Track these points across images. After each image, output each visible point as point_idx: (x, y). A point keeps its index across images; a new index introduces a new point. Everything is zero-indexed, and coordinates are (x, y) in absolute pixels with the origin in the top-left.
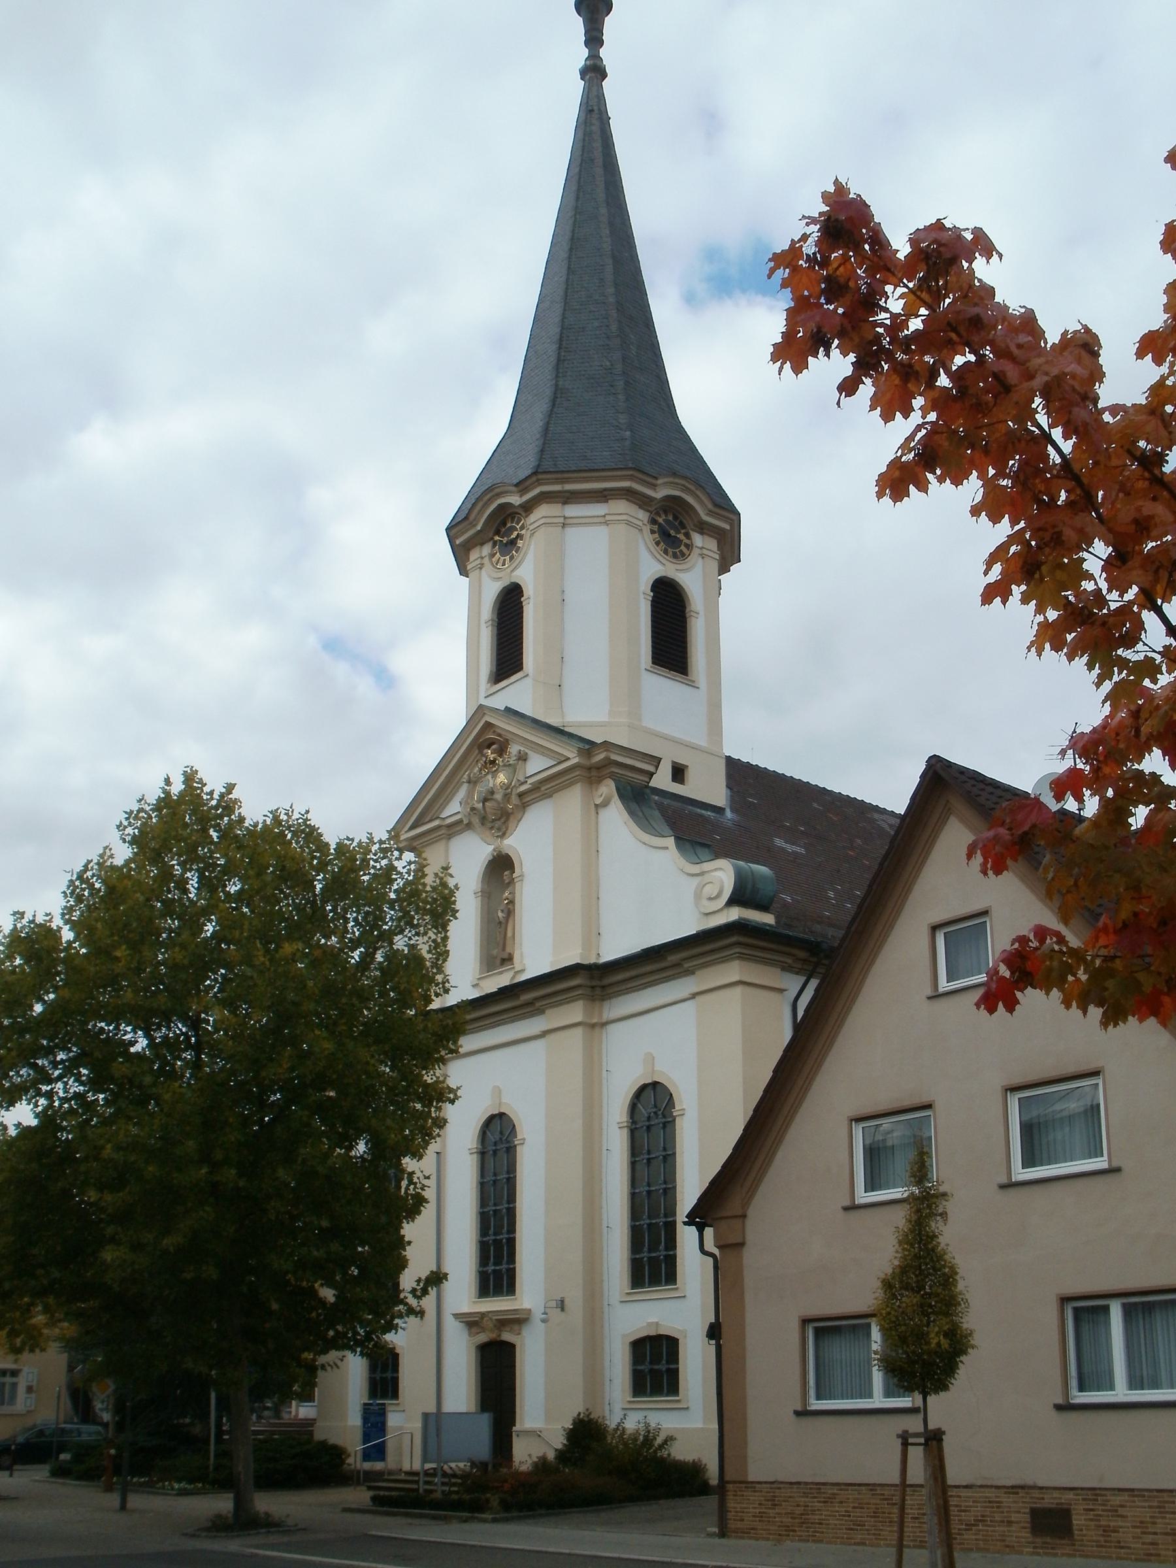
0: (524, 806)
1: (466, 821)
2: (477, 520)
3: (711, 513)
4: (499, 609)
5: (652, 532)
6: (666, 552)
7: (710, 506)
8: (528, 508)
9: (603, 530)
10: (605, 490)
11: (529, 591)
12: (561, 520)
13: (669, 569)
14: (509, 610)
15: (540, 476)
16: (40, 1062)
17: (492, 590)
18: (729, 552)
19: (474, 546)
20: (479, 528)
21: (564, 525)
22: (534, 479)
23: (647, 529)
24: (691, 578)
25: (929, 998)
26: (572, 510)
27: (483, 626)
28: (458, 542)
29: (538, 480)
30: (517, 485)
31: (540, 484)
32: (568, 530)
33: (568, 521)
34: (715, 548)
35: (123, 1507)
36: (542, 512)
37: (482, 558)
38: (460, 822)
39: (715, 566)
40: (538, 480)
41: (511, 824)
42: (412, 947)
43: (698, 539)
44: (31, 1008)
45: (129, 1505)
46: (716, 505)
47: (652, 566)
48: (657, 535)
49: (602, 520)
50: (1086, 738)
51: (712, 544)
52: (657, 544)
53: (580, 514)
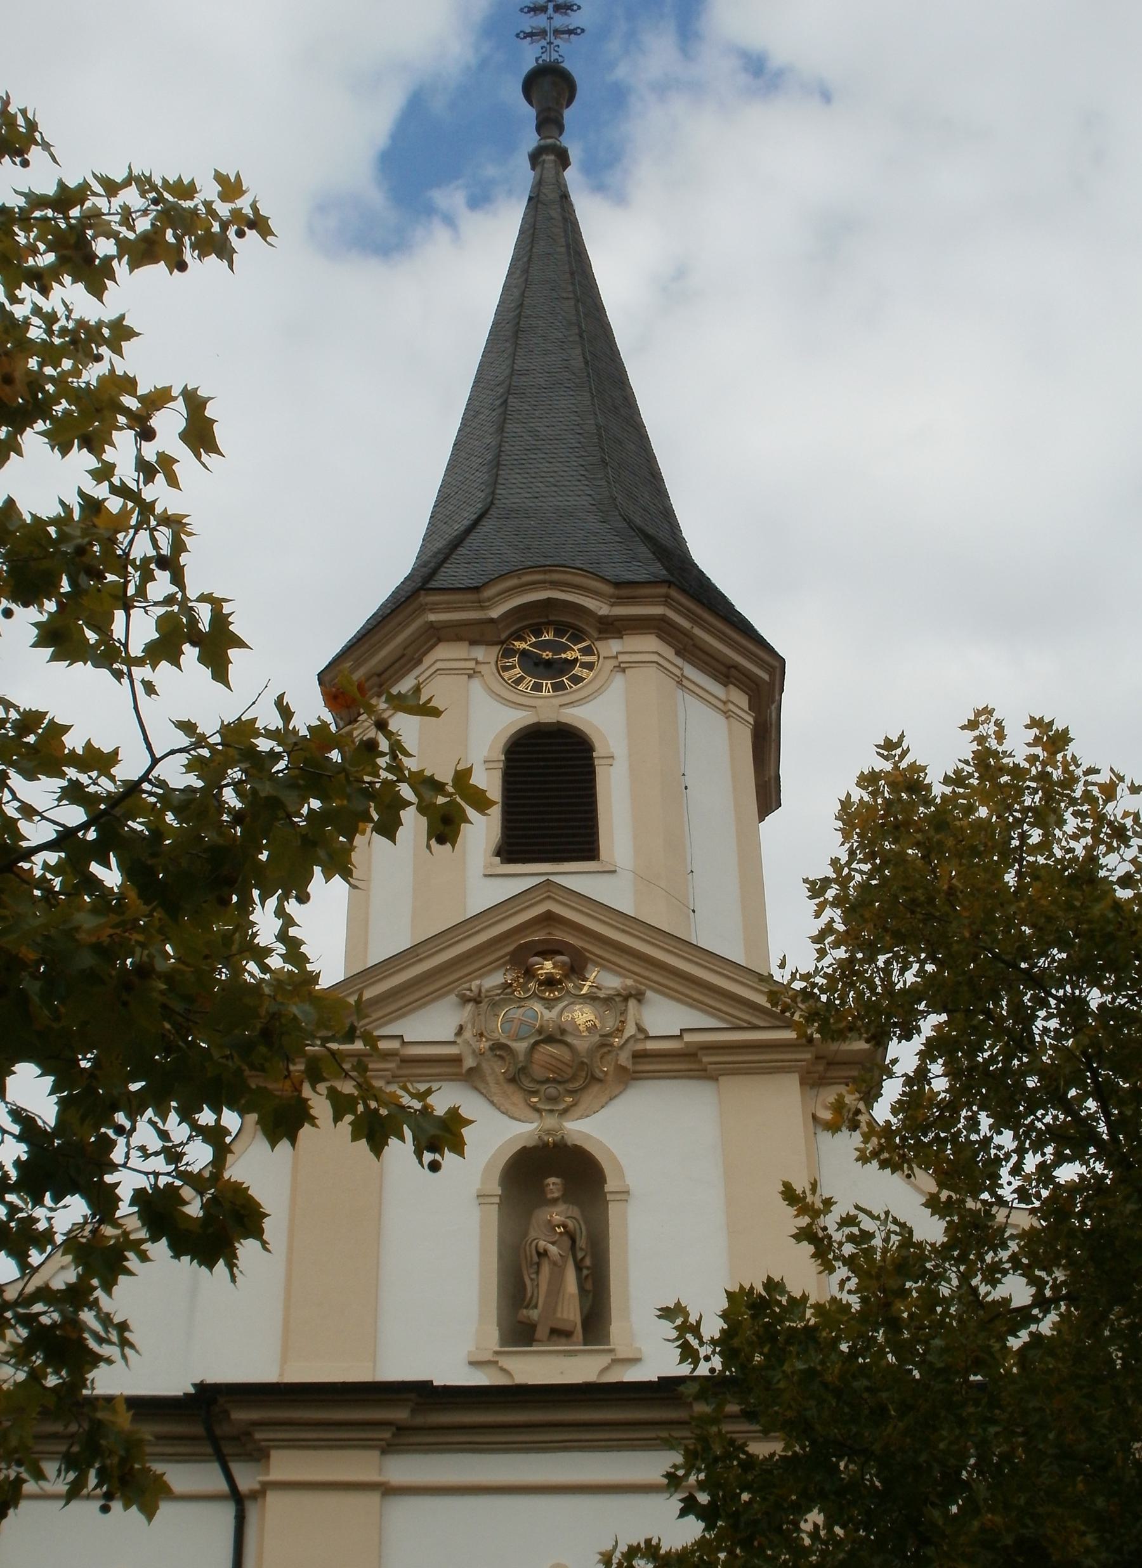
0: (628, 1077)
1: (469, 1062)
2: (493, 601)
3: (620, 600)
8: (612, 628)
10: (736, 667)
12: (472, 664)
13: (547, 706)
15: (673, 593)
19: (458, 639)
20: (494, 614)
21: (470, 676)
22: (663, 590)
25: (471, 1363)
29: (667, 596)
30: (617, 585)
31: (666, 604)
33: (685, 682)
38: (457, 1060)
40: (667, 596)
41: (587, 1099)
42: (1018, 1337)
44: (889, 1365)
46: (617, 585)
49: (720, 705)
53: (708, 688)
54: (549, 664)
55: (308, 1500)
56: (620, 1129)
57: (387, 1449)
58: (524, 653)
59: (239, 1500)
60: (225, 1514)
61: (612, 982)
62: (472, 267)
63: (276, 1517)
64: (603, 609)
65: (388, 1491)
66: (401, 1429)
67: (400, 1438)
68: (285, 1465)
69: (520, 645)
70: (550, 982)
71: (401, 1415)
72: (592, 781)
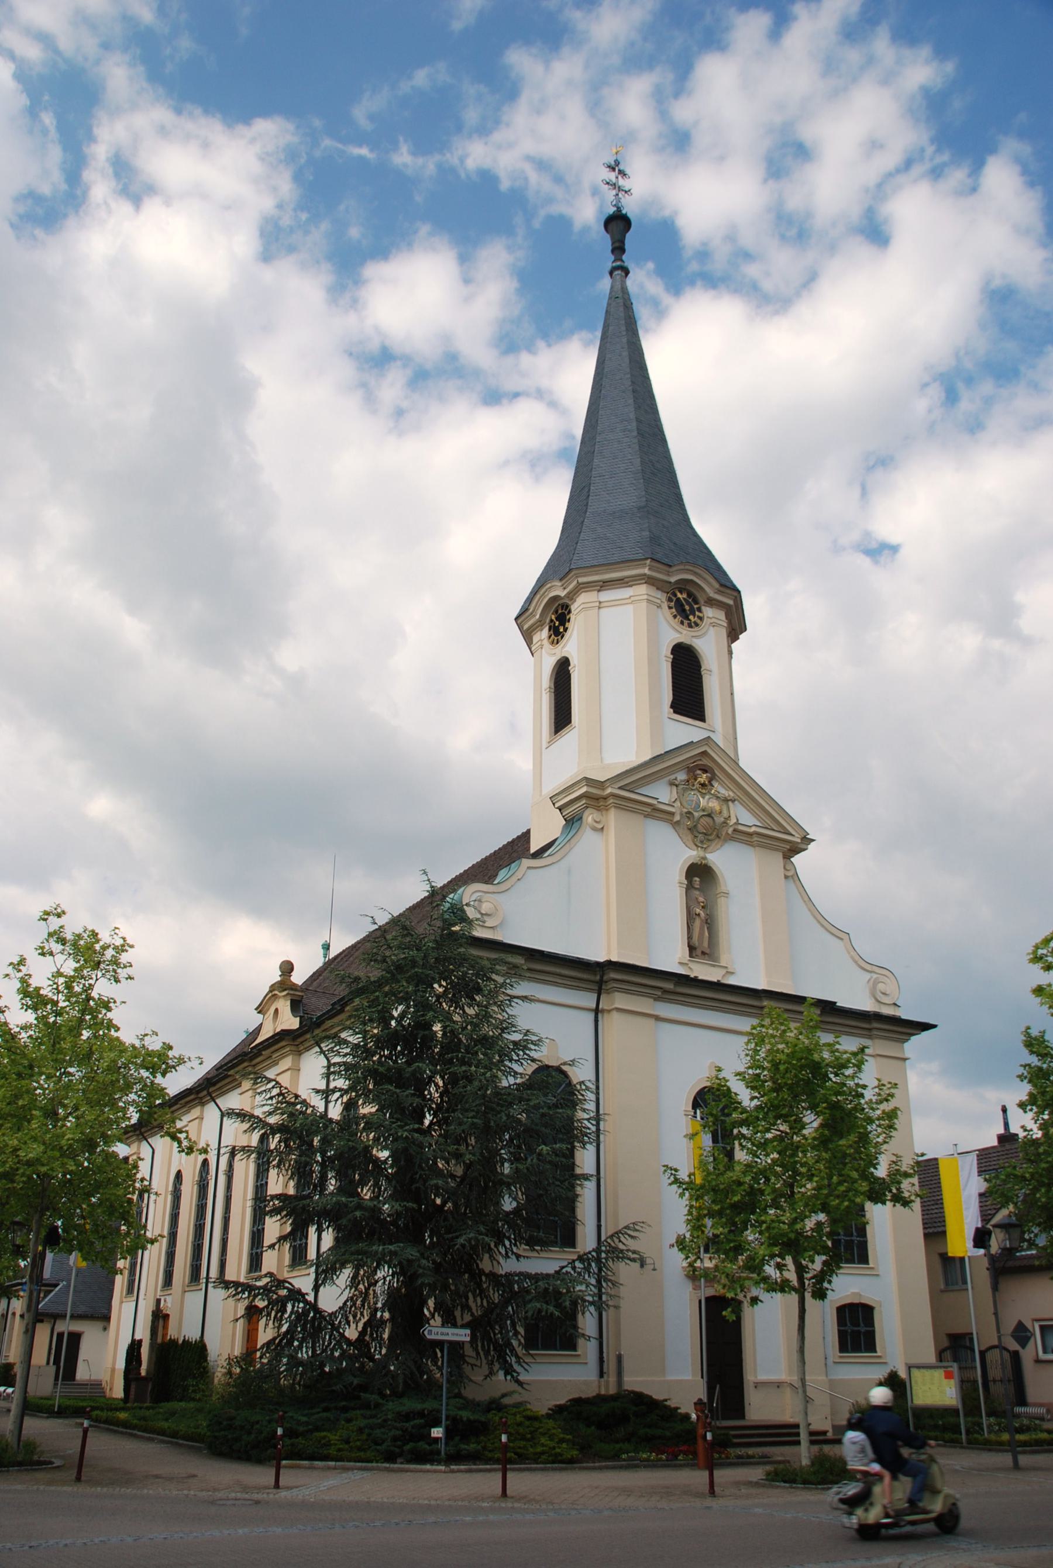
0: (730, 838)
3: (719, 592)
4: (557, 673)
5: (670, 608)
6: (682, 623)
7: (717, 586)
8: (572, 595)
9: (630, 607)
11: (574, 662)
13: (684, 636)
14: (562, 673)
16: (512, 1080)
17: (549, 663)
18: (736, 627)
23: (665, 605)
24: (707, 642)
26: (606, 596)
27: (544, 692)
28: (526, 627)
32: (601, 610)
34: (724, 618)
35: (277, 1485)
36: (583, 599)
37: (541, 640)
39: (723, 633)
43: (708, 612)
45: (282, 1482)
46: (722, 585)
47: (672, 633)
48: (674, 610)
50: (102, 1400)
51: (721, 615)
52: (675, 617)
53: (613, 598)
54: (684, 610)
55: (856, 1277)
56: (723, 859)
57: (657, 999)
58: (678, 600)
59: (597, 1011)
60: (591, 1016)
61: (724, 792)
62: (572, 373)
63: (614, 1026)
64: (712, 595)
65: (657, 1018)
66: (665, 991)
67: (665, 996)
68: (621, 1000)
69: (679, 595)
70: (703, 785)
71: (669, 986)
72: (701, 683)
